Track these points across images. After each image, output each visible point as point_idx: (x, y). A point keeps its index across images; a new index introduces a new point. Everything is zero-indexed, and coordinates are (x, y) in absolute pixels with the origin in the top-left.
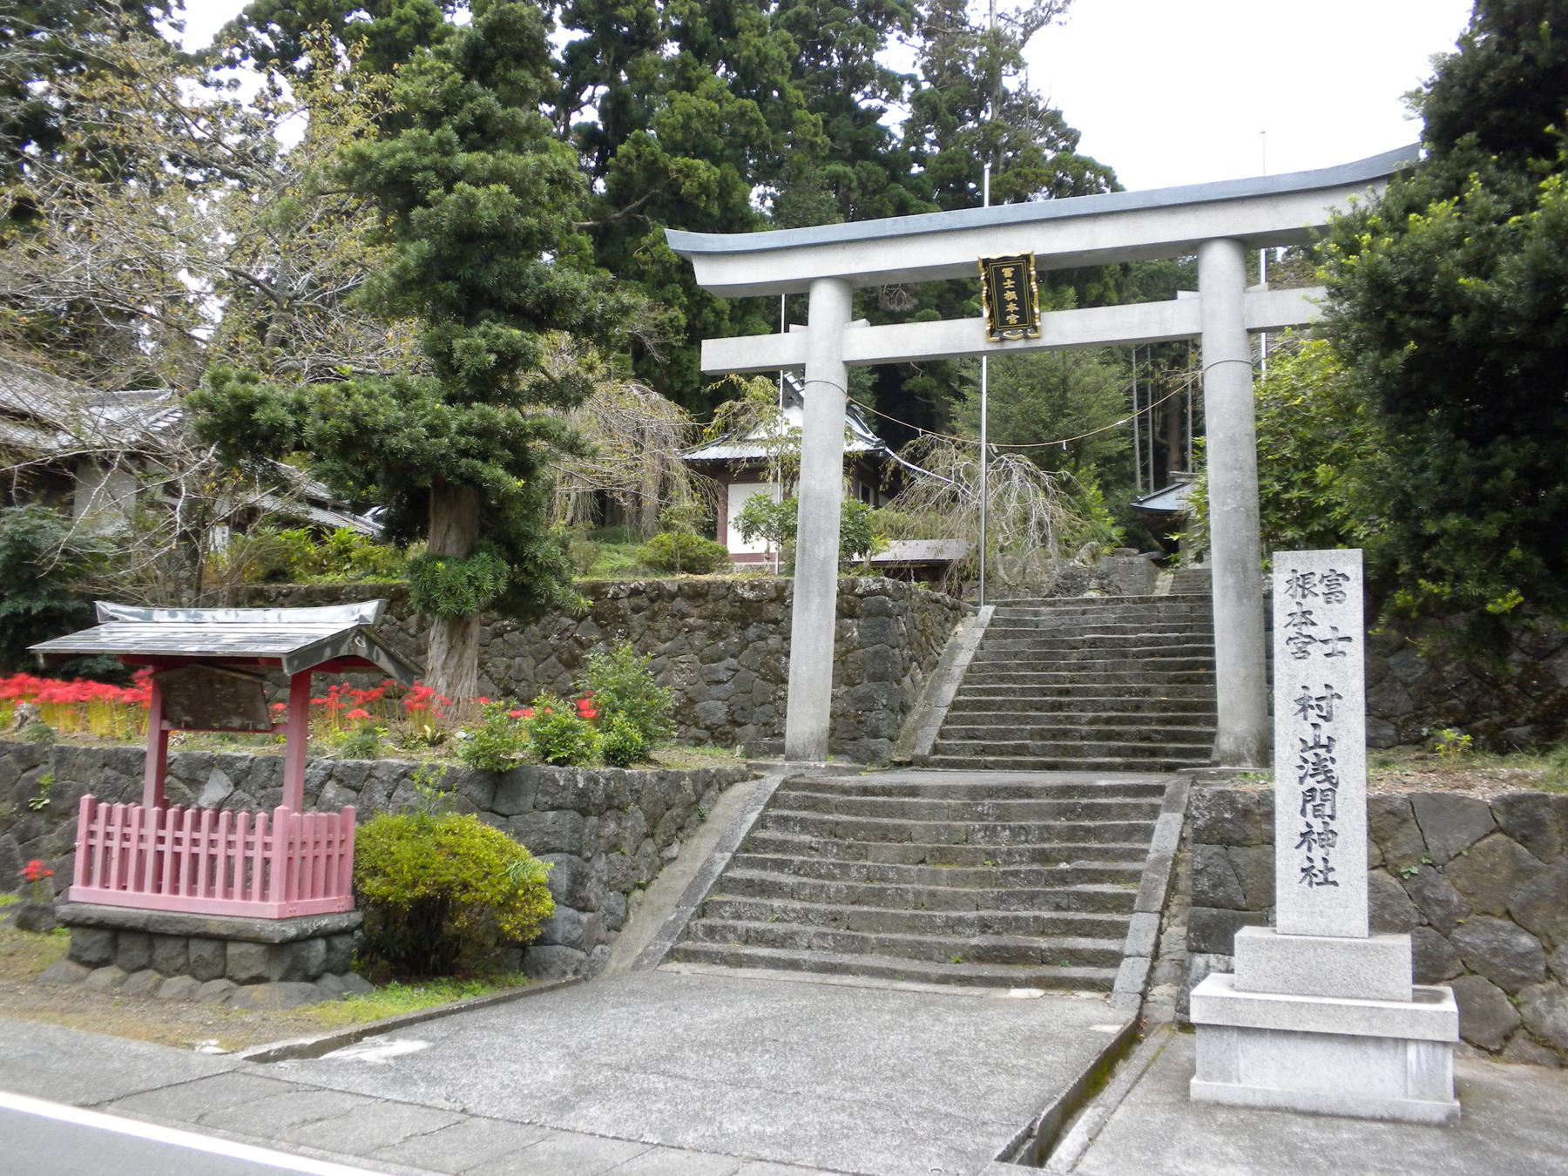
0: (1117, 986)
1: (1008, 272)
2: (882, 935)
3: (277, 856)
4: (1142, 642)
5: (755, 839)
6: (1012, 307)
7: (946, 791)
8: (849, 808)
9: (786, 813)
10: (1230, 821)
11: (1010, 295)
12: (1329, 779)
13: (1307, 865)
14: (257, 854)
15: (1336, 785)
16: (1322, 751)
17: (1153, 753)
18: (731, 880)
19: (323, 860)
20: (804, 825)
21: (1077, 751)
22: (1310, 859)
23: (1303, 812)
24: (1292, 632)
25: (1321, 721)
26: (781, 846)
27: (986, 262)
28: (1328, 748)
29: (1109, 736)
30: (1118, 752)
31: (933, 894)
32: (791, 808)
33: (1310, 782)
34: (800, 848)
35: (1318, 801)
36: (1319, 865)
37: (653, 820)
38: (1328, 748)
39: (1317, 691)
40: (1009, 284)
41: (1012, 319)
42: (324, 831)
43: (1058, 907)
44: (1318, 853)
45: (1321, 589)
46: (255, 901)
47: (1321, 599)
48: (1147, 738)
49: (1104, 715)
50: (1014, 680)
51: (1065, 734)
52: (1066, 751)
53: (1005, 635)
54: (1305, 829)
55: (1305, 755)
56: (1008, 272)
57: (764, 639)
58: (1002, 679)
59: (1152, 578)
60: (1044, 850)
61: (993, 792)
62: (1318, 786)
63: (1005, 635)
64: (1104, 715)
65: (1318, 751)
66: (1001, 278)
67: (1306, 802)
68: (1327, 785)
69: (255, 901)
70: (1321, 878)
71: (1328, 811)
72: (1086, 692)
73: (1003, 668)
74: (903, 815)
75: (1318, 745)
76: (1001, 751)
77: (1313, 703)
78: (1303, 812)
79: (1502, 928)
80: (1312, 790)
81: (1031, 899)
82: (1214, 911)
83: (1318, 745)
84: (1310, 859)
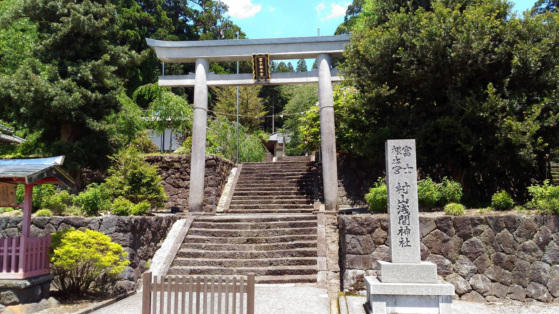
0: (318, 280)
1: (261, 60)
2: (237, 268)
3: (21, 255)
4: (287, 175)
5: (187, 239)
6: (261, 71)
7: (249, 220)
8: (218, 227)
9: (197, 229)
10: (357, 227)
11: (261, 67)
12: (407, 212)
13: (401, 240)
14: (13, 254)
15: (409, 214)
16: (404, 204)
17: (297, 207)
18: (181, 253)
19: (34, 256)
20: (203, 233)
21: (274, 207)
22: (402, 239)
23: (399, 223)
24: (394, 165)
25: (404, 194)
26: (197, 240)
27: (254, 56)
28: (407, 202)
29: (283, 203)
30: (286, 207)
31: (251, 254)
32: (197, 227)
33: (401, 213)
34: (204, 241)
35: (404, 220)
36: (405, 240)
37: (154, 234)
38: (407, 202)
39: (403, 184)
40: (261, 63)
41: (262, 74)
42: (39, 244)
43: (292, 256)
44: (405, 236)
45: (403, 152)
46: (13, 272)
47: (403, 155)
48: (294, 203)
49: (280, 196)
50: (251, 186)
51: (270, 202)
52: (270, 207)
53: (246, 173)
54: (400, 229)
55: (399, 205)
56: (261, 60)
57: (174, 174)
58: (248, 186)
59: (272, 159)
60: (284, 238)
61: (264, 220)
62: (404, 215)
63: (246, 173)
64: (280, 196)
65: (403, 203)
66: (259, 61)
67: (400, 220)
68: (406, 214)
69: (13, 272)
70: (406, 244)
71: (407, 223)
72: (274, 190)
73: (247, 182)
74: (236, 228)
75: (403, 201)
76: (251, 208)
77: (401, 188)
78: (399, 223)
79: (440, 258)
80: (402, 216)
81: (284, 254)
82: (354, 256)
83: (403, 201)
84: (402, 239)
